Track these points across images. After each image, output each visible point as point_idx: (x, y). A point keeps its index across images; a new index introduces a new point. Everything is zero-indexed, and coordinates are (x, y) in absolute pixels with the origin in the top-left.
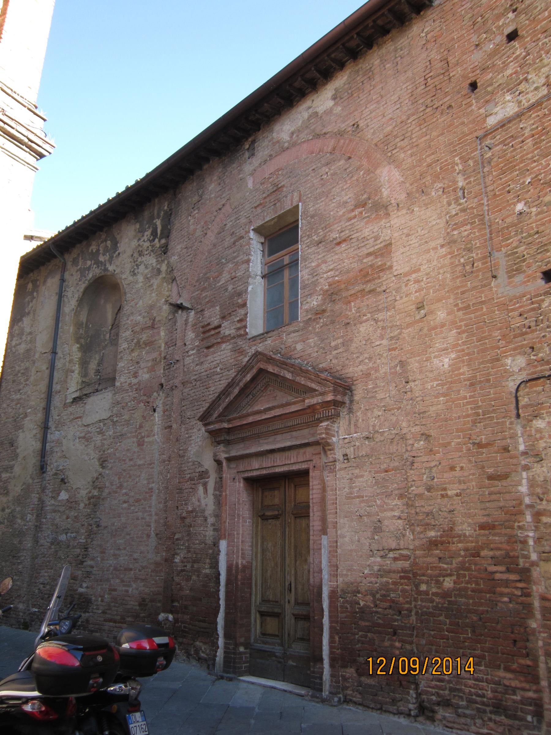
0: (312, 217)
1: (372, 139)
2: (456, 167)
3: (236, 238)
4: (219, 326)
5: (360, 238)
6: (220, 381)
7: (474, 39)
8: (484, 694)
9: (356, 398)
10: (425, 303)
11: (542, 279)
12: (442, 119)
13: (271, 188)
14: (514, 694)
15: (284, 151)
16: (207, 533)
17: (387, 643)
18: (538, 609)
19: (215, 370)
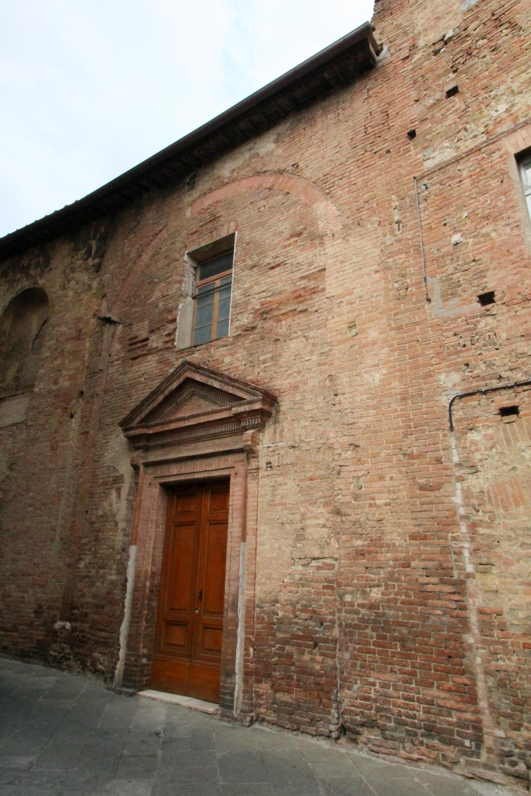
0: (248, 244)
1: (311, 178)
2: (393, 204)
4: (147, 339)
7: (414, 95)
8: (415, 715)
9: (282, 409)
10: (357, 323)
12: (381, 162)
13: (208, 217)
14: (450, 715)
15: (224, 185)
16: (117, 538)
17: (307, 657)
18: (476, 623)
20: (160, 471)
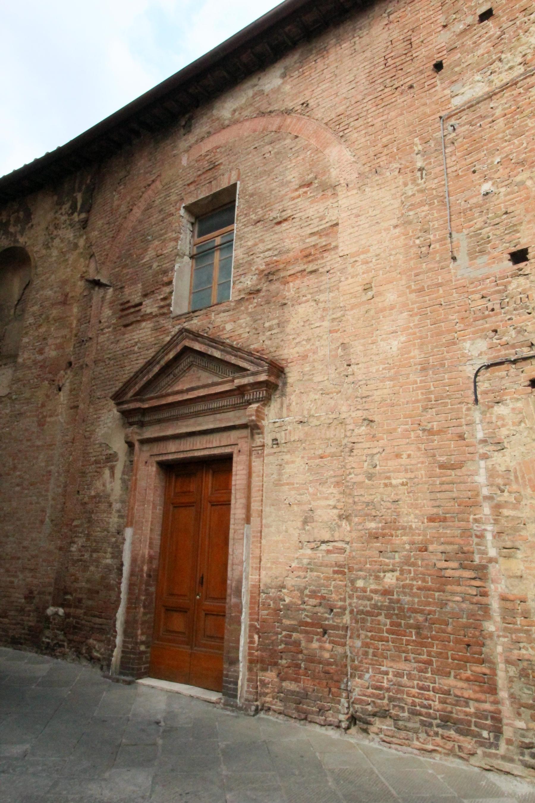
0: (252, 195)
2: (415, 148)
3: (164, 215)
4: (140, 304)
5: (303, 218)
6: (137, 360)
7: (441, 19)
8: (430, 705)
10: (373, 285)
11: (509, 260)
12: (402, 100)
13: (206, 165)
15: (224, 128)
19: (132, 348)
20: (156, 449)
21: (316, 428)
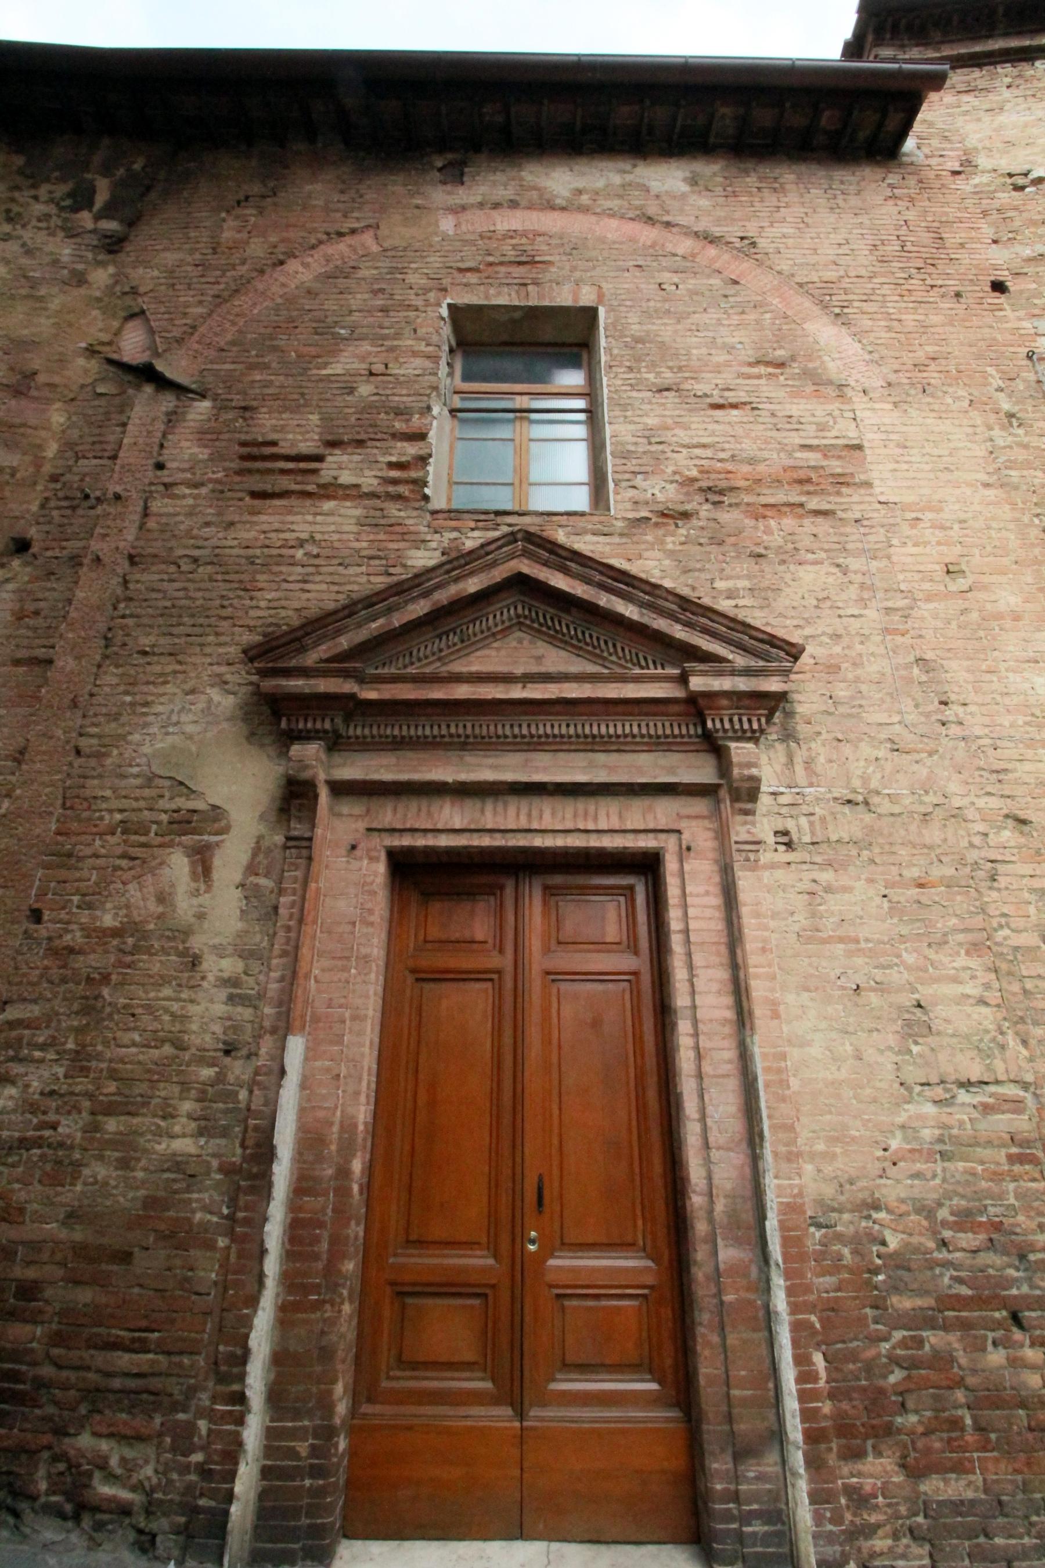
4: (319, 458)
16: (193, 1009)
19: (291, 552)
20: (388, 814)
21: (892, 819)
